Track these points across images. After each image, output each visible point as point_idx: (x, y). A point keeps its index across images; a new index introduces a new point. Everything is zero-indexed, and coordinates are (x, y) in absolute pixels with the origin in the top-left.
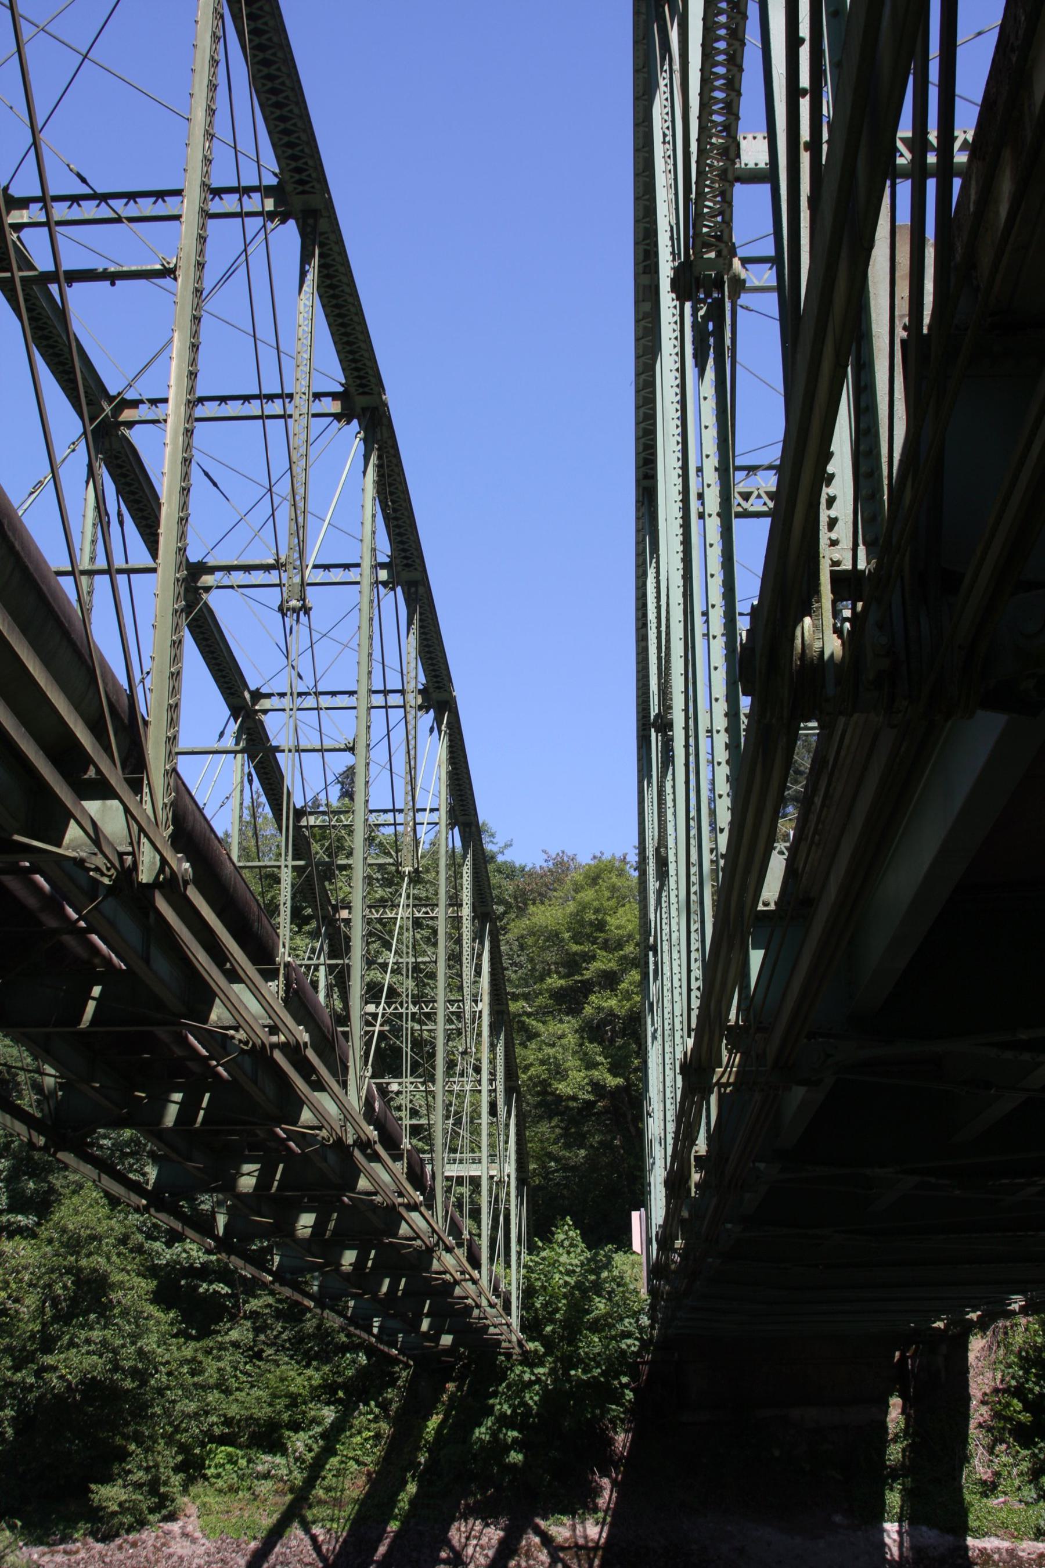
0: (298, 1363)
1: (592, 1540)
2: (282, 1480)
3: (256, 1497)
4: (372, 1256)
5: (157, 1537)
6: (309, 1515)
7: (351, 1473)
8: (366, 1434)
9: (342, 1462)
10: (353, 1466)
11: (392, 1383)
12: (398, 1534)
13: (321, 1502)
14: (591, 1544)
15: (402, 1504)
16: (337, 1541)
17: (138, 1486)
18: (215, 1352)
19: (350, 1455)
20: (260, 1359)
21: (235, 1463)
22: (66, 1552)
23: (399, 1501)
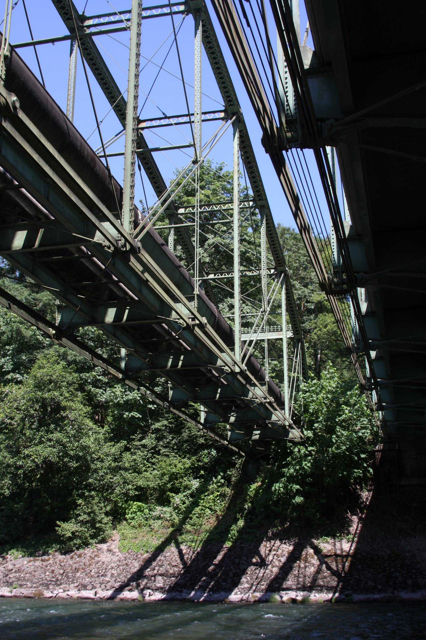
1: (345, 551)
2: (167, 520)
3: (152, 530)
4: (219, 392)
5: (93, 552)
6: (180, 539)
7: (207, 516)
9: (202, 509)
10: (208, 512)
11: (233, 465)
12: (230, 549)
13: (188, 532)
14: (344, 554)
15: (233, 532)
16: (193, 553)
17: (83, 523)
18: (132, 450)
19: (207, 506)
20: (159, 454)
22: (42, 560)
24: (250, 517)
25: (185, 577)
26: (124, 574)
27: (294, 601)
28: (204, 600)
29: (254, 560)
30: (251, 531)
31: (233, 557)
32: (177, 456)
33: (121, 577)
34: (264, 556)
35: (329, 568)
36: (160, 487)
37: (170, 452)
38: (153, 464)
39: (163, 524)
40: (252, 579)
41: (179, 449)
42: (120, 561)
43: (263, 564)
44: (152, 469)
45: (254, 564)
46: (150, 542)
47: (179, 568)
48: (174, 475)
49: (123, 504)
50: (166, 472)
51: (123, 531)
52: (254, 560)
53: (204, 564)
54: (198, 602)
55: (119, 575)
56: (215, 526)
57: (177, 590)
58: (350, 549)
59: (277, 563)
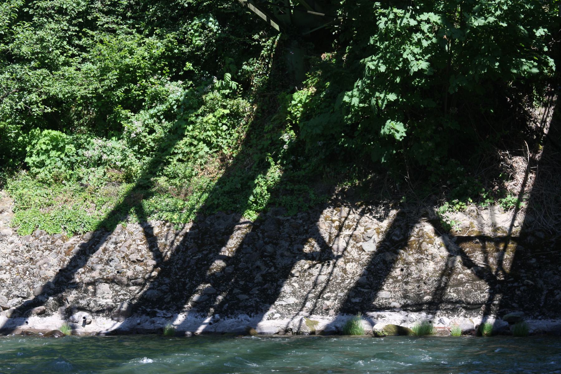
0: (139, 32)
2: (116, 167)
3: (84, 187)
6: (146, 204)
7: (202, 157)
8: (221, 111)
9: (191, 144)
11: (255, 52)
14: (500, 234)
18: (35, 19)
21: (62, 149)
23: (255, 186)
24: (293, 159)
25: (160, 284)
26: (27, 281)
27: (401, 332)
28: (204, 332)
29: (307, 249)
30: (297, 187)
31: (261, 242)
32: (134, 31)
33: (20, 286)
34: (327, 240)
35: (468, 263)
36: (99, 97)
37: (117, 23)
38: (82, 49)
39: (108, 175)
40: (302, 286)
41: (137, 18)
42: (16, 253)
43: (325, 255)
44: (80, 60)
45: (307, 257)
46: (80, 212)
47: (146, 265)
48: (129, 72)
49: (18, 135)
50: (111, 65)
51: (20, 191)
52: (307, 249)
53: (200, 256)
54: (193, 335)
55: (15, 282)
56: (220, 180)
57: (144, 312)
58: (512, 225)
59: (354, 253)
